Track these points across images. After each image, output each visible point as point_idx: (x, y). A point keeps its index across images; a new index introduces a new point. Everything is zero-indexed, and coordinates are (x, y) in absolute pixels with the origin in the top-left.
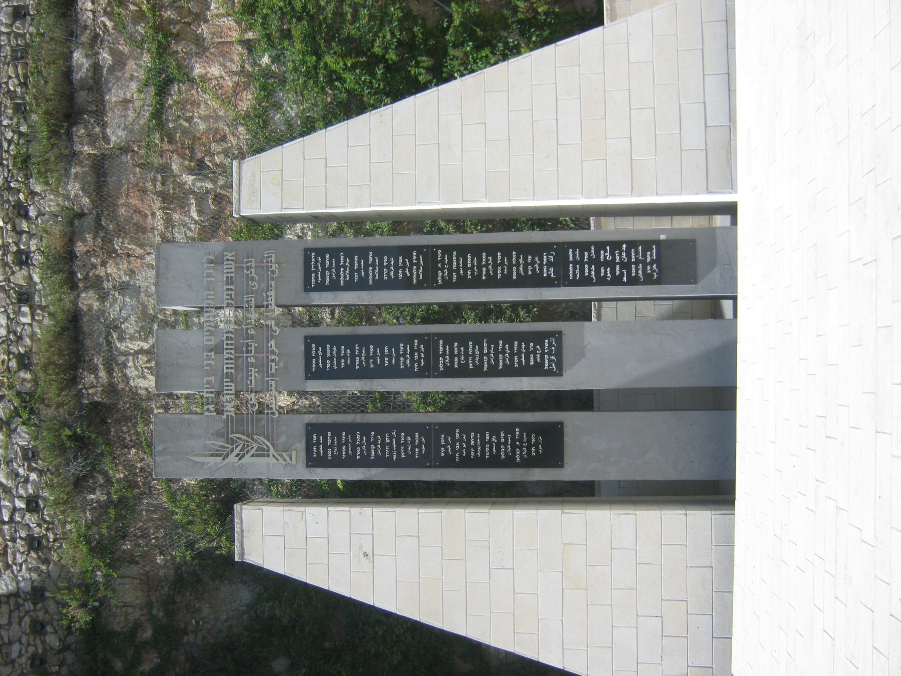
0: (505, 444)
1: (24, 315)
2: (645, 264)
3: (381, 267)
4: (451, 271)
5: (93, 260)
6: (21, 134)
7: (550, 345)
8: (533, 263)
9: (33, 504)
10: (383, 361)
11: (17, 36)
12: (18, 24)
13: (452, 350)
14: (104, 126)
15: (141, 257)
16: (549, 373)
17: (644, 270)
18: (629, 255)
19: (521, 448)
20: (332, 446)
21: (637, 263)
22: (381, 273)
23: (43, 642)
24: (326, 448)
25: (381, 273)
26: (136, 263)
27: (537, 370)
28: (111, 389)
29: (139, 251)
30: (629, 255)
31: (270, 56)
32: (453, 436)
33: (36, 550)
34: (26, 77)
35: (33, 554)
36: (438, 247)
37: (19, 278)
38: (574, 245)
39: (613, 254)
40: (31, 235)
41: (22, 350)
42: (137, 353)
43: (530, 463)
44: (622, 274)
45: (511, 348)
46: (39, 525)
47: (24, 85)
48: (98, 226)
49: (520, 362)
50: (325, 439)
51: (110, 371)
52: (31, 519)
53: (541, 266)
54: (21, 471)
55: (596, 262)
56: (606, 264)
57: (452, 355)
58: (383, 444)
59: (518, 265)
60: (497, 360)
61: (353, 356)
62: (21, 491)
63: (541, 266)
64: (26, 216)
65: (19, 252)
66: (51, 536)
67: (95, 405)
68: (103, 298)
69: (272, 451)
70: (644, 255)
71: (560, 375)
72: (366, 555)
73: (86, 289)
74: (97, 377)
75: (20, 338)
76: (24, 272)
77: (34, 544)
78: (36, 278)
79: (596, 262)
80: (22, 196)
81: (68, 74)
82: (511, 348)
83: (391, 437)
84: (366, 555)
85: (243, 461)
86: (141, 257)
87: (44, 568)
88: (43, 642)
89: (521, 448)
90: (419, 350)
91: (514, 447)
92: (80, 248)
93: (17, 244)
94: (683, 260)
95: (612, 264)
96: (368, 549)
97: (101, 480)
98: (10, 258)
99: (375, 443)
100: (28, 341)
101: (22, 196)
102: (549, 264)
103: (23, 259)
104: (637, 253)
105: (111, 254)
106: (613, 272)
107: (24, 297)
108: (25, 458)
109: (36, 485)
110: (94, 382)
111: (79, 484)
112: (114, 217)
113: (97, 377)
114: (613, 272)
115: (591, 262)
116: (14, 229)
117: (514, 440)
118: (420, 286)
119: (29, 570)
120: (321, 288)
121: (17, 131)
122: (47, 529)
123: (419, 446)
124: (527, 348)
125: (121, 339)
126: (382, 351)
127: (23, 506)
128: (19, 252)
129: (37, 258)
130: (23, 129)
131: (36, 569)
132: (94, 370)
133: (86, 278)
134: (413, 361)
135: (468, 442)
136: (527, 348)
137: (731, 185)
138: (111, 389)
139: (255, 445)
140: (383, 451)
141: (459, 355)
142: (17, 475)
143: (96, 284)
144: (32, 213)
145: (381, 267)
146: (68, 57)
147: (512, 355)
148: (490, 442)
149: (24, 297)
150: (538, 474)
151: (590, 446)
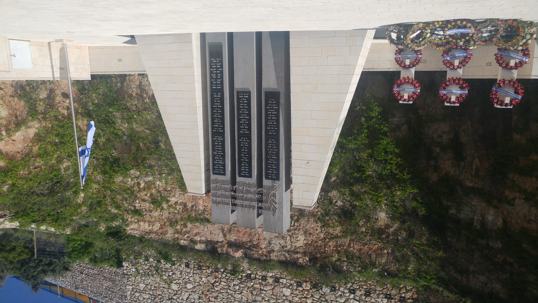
0: (272, 112)
1: (283, 281)
2: (216, 63)
3: (218, 150)
4: (219, 127)
5: (260, 252)
6: (224, 271)
7: (241, 95)
8: (216, 100)
9: (352, 291)
10: (246, 152)
11: (194, 267)
12: (190, 266)
13: (243, 128)
14: (218, 242)
15: (259, 235)
16: (250, 96)
17: (218, 63)
18: (214, 68)
19: (273, 107)
20: (272, 171)
21: (216, 65)
22: (220, 150)
23: (409, 299)
24: (273, 173)
25: (220, 150)
26: (261, 237)
27: (249, 100)
28: (305, 254)
29: (257, 235)
30: (214, 68)
31: (392, 206)
32: (270, 130)
33: (370, 294)
34: (206, 266)
35: (372, 295)
36: (212, 131)
37: (270, 281)
38: (211, 86)
39: (214, 74)
40: (256, 274)
41: (295, 285)
42: (291, 242)
43: (278, 104)
44: (220, 71)
45: (242, 108)
46: (360, 291)
47: (209, 267)
48: (249, 248)
49: (246, 106)
50: (270, 173)
51: (297, 253)
52: (358, 293)
53: (217, 97)
54: (340, 293)
55: (216, 79)
56: (217, 76)
57: (244, 128)
58: (272, 153)
59: (217, 105)
60: (246, 114)
61: (245, 161)
62: (348, 295)
63: (217, 97)
64: (250, 274)
65: (262, 279)
66: (365, 287)
67: (310, 260)
68: (273, 251)
69: (274, 192)
70: (214, 63)
71: (250, 92)
72: (308, 163)
73: (270, 256)
74: (300, 258)
75: (291, 285)
76: (268, 278)
78: (271, 275)
79: (216, 79)
80: (244, 275)
81: (204, 251)
82: (242, 108)
83: (270, 151)
84: (308, 163)
85: (277, 202)
86: (259, 235)
87: (377, 292)
88: (409, 299)
89: (273, 107)
90: (243, 139)
91: (273, 109)
92: (256, 256)
93: (259, 279)
94: (217, 53)
95: (217, 74)
96: (306, 162)
97: (338, 263)
98: (263, 283)
99: (271, 156)
100: (292, 282)
101: (244, 275)
102: (217, 95)
103: (264, 278)
104: (213, 65)
105: (257, 246)
106: (219, 73)
107: (277, 280)
108: (335, 291)
109: (346, 288)
110: (303, 260)
111: (338, 270)
112: (246, 243)
113: (300, 258)
114: (219, 73)
115: (216, 81)
116: (254, 279)
117: (271, 109)
118: (224, 137)
119: (378, 298)
120: (224, 170)
121: (223, 273)
122: (362, 288)
123: (273, 141)
124: (242, 103)
125: (286, 247)
126: (243, 152)
127: (353, 295)
128: (262, 279)
129: (264, 273)
130: (222, 270)
131: (378, 295)
132: (298, 258)
133: (266, 256)
134: (246, 142)
135: (271, 125)
136: (242, 103)
137: (185, 38)
138: (305, 254)
139: (272, 197)
140: (274, 154)
141: (244, 126)
142: (341, 295)
143: (270, 252)
144: (249, 272)
145: (218, 150)
146: (198, 251)
147: (244, 108)
148: (271, 117)
149: (277, 280)
150: (282, 101)
151: (270, 82)
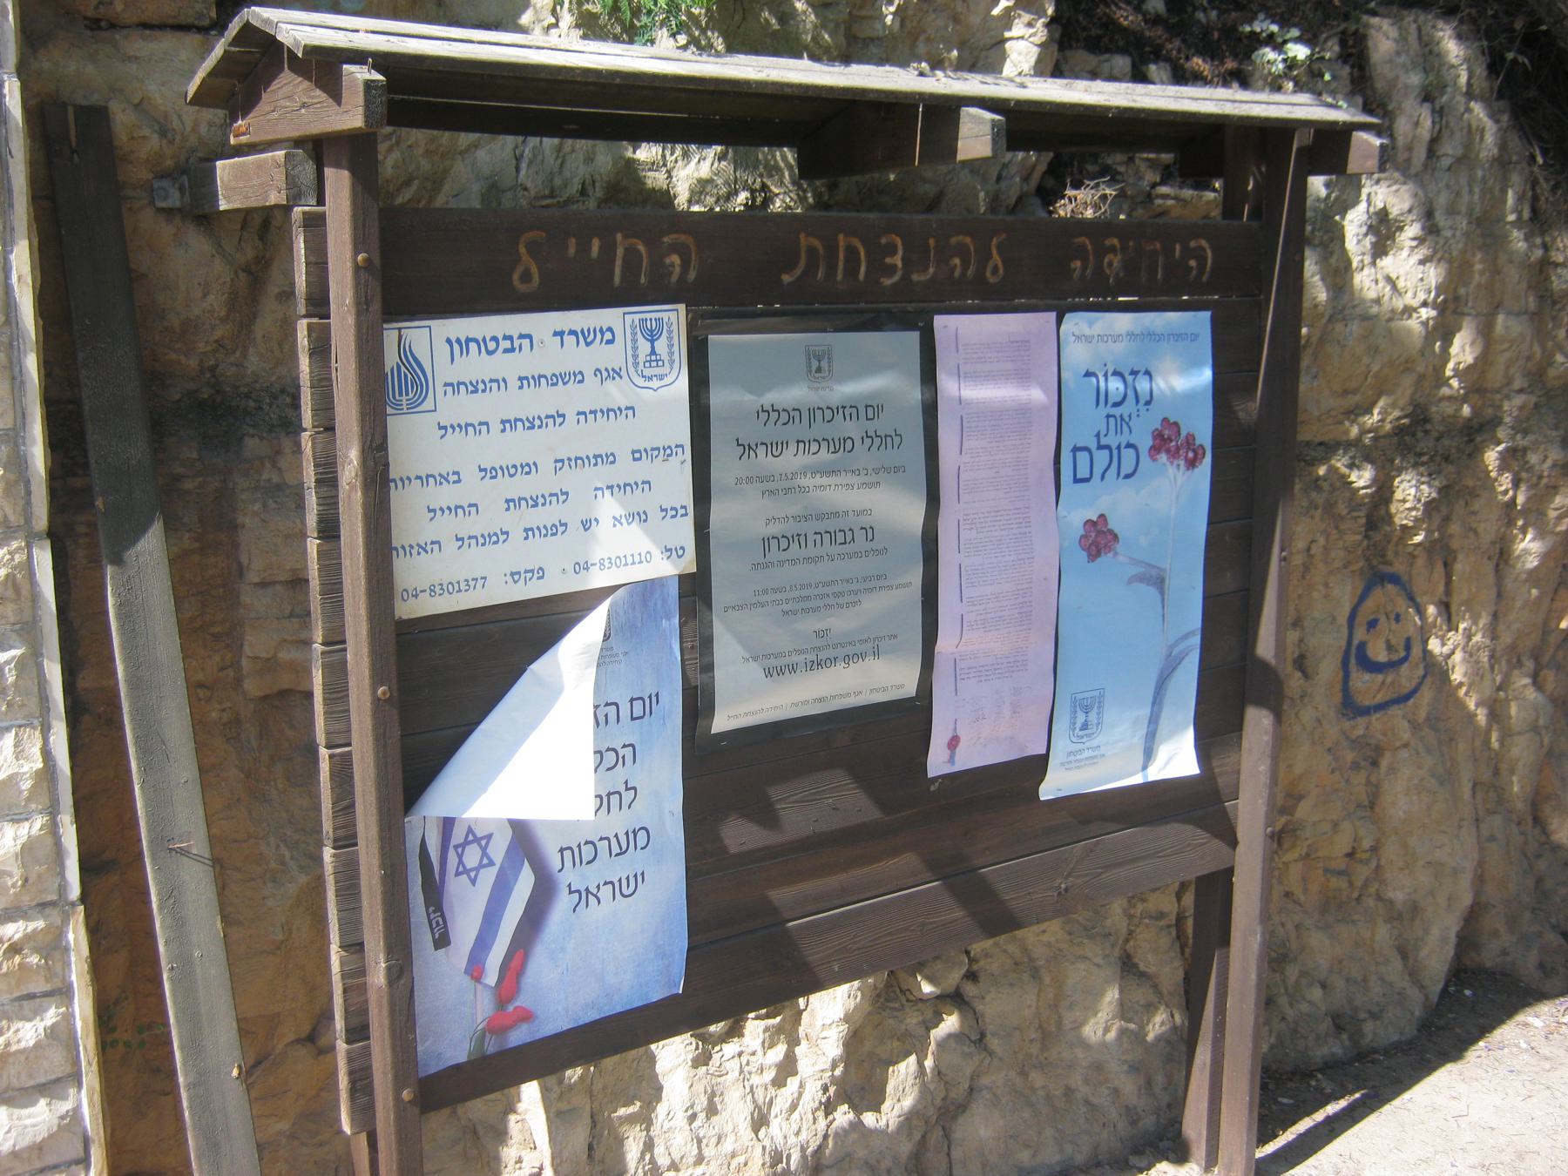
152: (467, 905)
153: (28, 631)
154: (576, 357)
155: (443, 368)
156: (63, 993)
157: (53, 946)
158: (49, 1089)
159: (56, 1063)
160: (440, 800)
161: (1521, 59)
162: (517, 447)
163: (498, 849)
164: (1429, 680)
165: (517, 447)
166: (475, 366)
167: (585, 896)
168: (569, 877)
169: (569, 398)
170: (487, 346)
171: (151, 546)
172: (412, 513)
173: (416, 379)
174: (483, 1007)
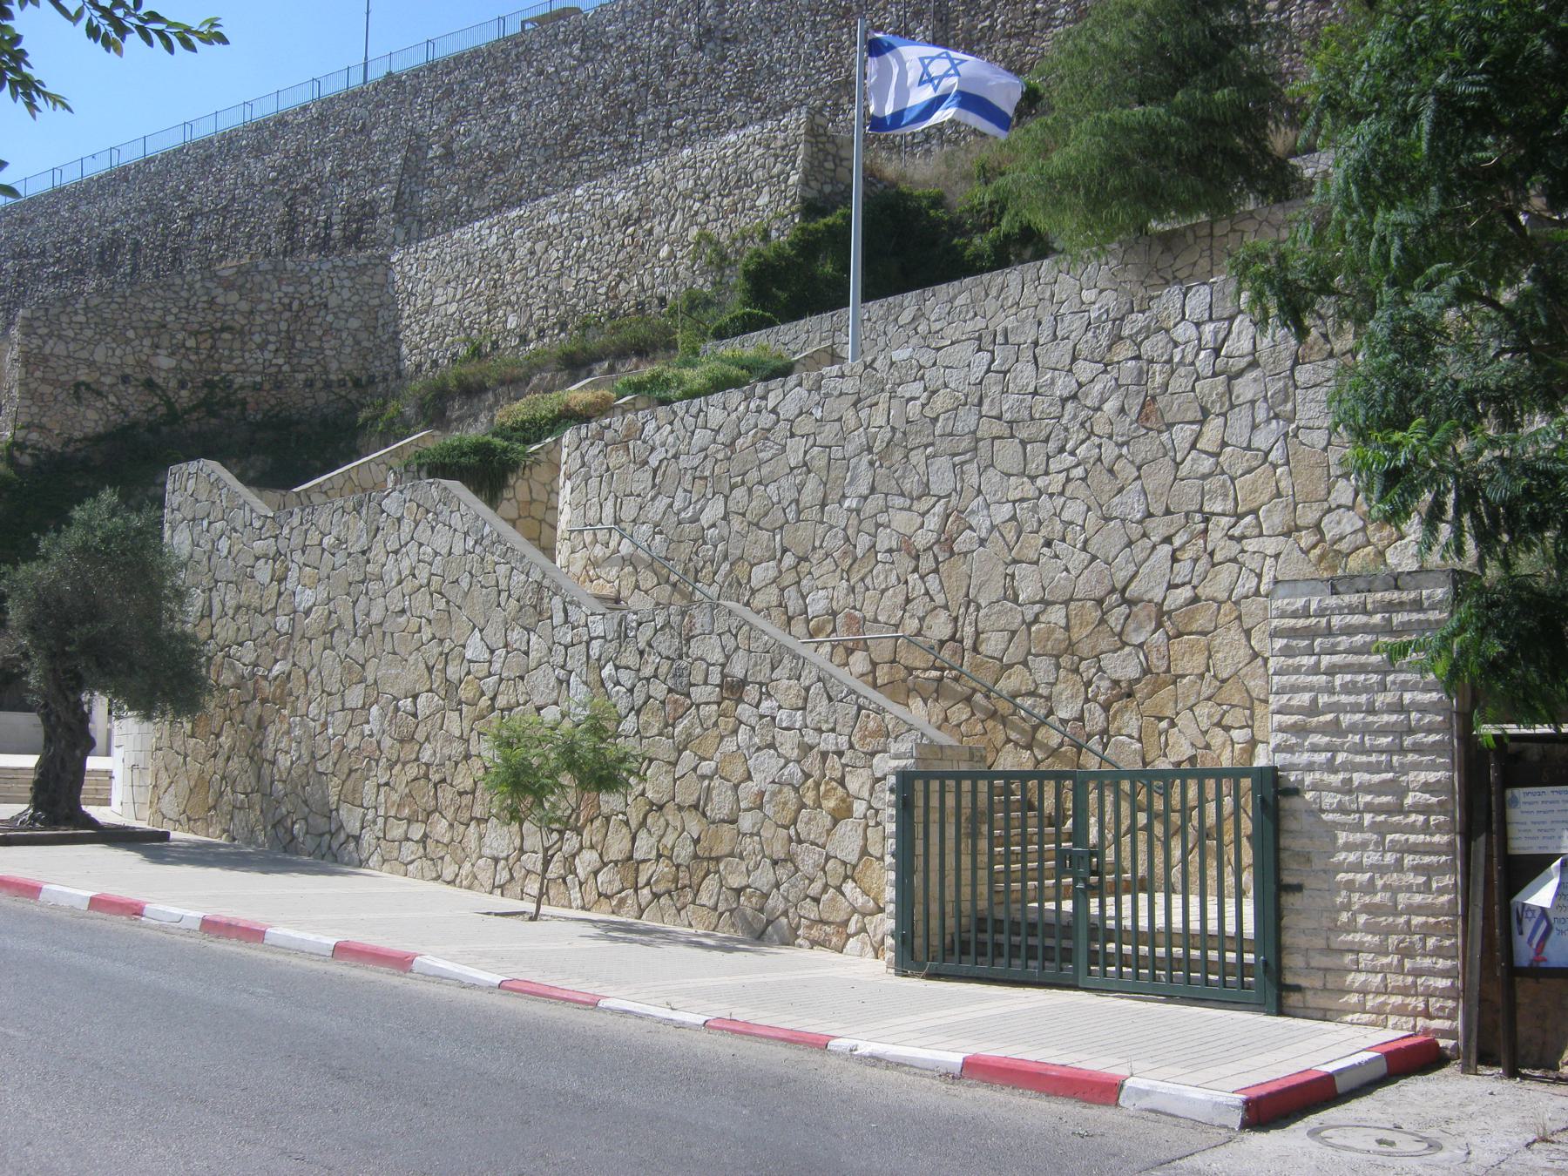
52: (428, 365)
77: (419, 366)
152: (1528, 926)
153: (1454, 853)
154: (1557, 797)
155: (1522, 799)
156: (1456, 936)
157: (1455, 924)
158: (1452, 958)
159: (1453, 952)
160: (1518, 898)
161: (1394, 216)
162: (1542, 817)
163: (1537, 914)
164: (1189, 629)
165: (1542, 817)
166: (1530, 798)
167: (1561, 932)
168: (1556, 925)
169: (1555, 807)
170: (1534, 794)
171: (1482, 839)
172: (1513, 831)
173: (1515, 801)
174: (1532, 954)
